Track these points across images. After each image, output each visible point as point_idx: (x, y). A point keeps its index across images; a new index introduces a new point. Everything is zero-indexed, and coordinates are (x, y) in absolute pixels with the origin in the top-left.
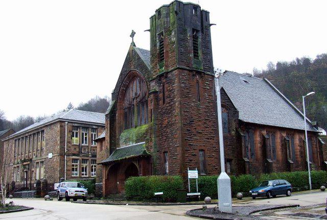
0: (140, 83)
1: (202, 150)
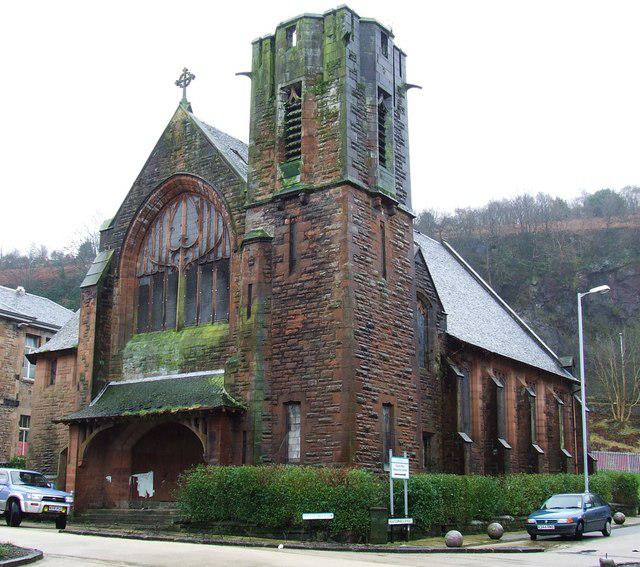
0: (200, 211)
1: (388, 405)
